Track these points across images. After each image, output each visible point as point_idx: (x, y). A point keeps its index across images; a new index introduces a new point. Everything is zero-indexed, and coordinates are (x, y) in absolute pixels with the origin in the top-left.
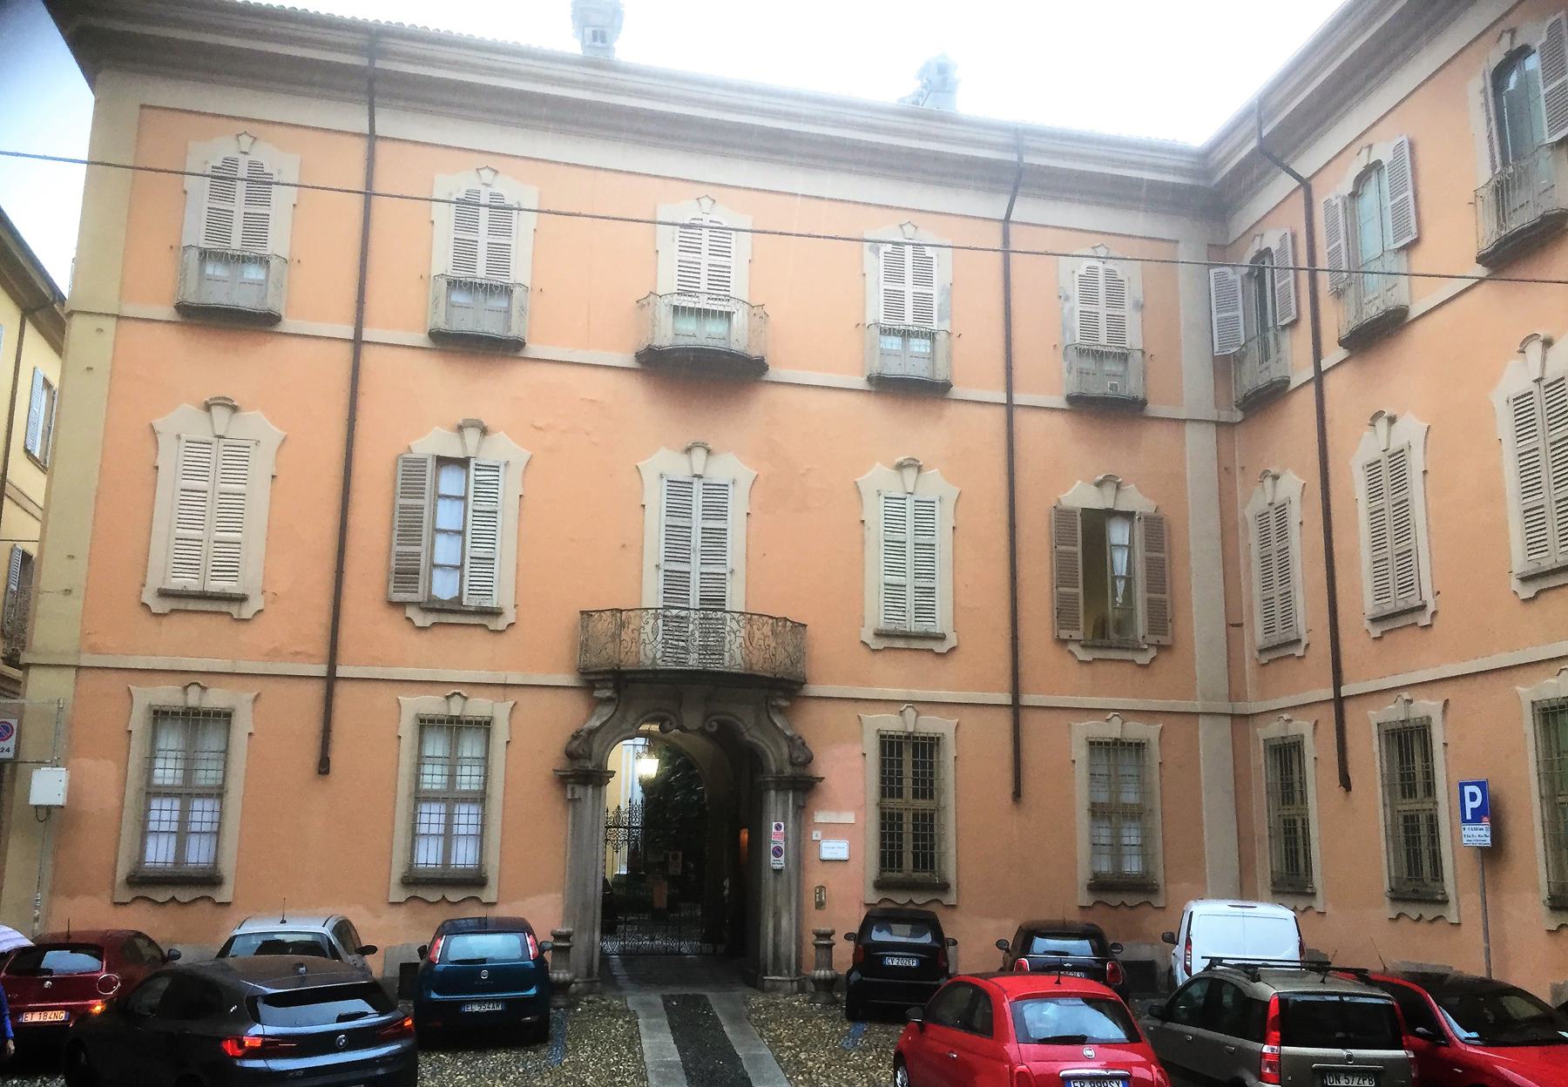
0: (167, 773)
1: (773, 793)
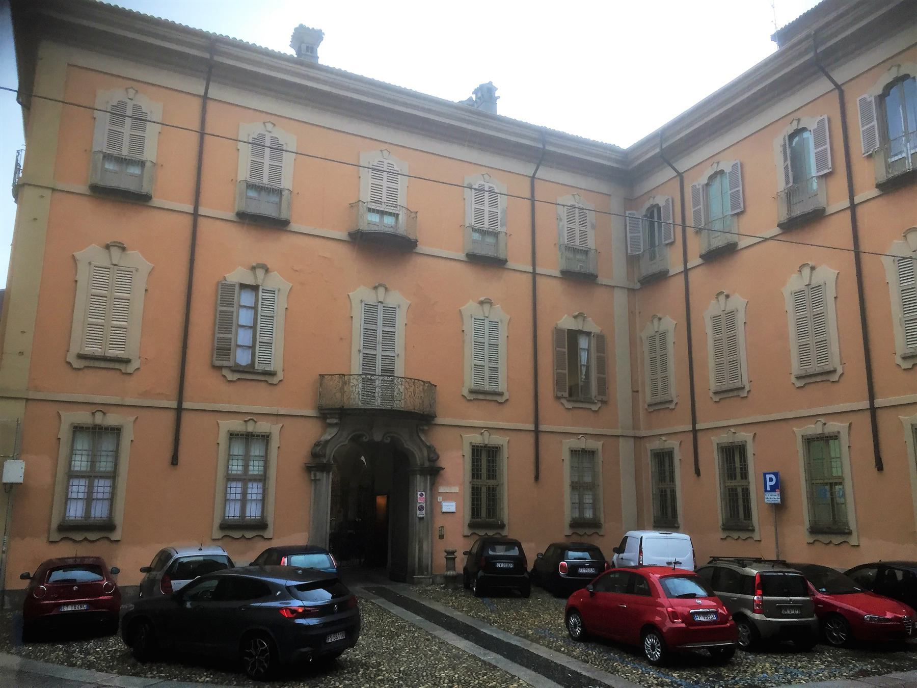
0: (80, 464)
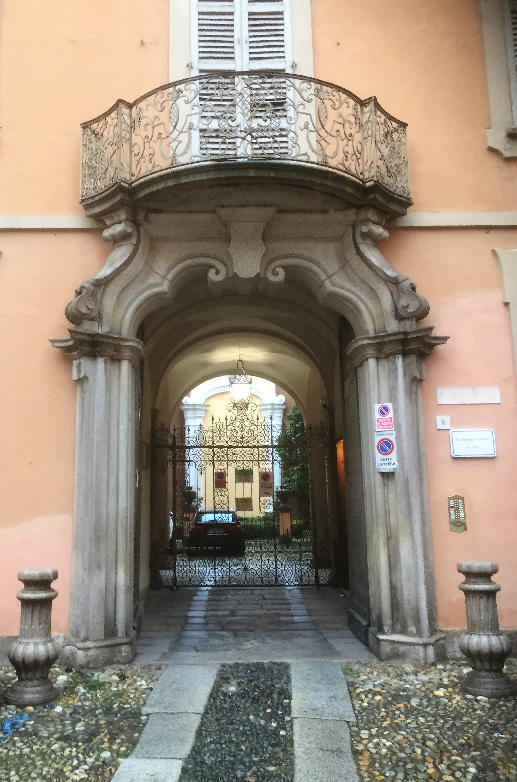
1: (372, 362)
